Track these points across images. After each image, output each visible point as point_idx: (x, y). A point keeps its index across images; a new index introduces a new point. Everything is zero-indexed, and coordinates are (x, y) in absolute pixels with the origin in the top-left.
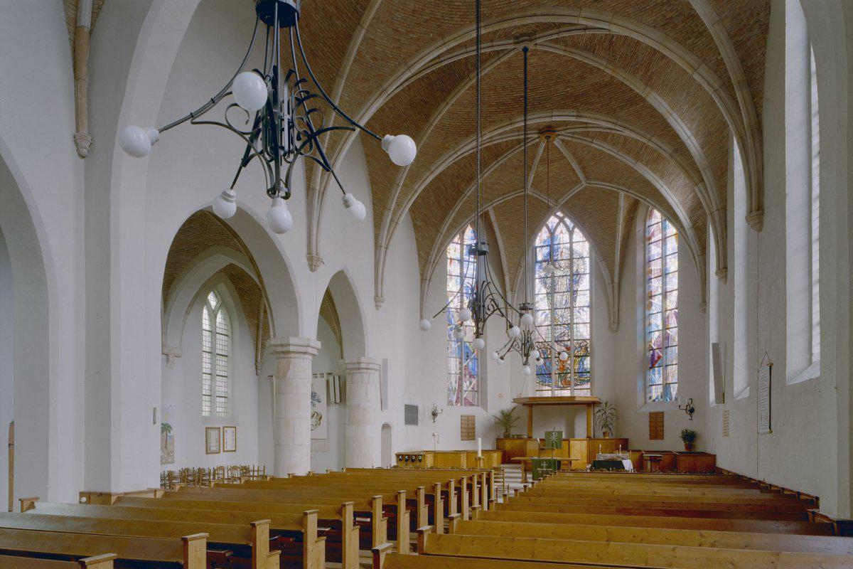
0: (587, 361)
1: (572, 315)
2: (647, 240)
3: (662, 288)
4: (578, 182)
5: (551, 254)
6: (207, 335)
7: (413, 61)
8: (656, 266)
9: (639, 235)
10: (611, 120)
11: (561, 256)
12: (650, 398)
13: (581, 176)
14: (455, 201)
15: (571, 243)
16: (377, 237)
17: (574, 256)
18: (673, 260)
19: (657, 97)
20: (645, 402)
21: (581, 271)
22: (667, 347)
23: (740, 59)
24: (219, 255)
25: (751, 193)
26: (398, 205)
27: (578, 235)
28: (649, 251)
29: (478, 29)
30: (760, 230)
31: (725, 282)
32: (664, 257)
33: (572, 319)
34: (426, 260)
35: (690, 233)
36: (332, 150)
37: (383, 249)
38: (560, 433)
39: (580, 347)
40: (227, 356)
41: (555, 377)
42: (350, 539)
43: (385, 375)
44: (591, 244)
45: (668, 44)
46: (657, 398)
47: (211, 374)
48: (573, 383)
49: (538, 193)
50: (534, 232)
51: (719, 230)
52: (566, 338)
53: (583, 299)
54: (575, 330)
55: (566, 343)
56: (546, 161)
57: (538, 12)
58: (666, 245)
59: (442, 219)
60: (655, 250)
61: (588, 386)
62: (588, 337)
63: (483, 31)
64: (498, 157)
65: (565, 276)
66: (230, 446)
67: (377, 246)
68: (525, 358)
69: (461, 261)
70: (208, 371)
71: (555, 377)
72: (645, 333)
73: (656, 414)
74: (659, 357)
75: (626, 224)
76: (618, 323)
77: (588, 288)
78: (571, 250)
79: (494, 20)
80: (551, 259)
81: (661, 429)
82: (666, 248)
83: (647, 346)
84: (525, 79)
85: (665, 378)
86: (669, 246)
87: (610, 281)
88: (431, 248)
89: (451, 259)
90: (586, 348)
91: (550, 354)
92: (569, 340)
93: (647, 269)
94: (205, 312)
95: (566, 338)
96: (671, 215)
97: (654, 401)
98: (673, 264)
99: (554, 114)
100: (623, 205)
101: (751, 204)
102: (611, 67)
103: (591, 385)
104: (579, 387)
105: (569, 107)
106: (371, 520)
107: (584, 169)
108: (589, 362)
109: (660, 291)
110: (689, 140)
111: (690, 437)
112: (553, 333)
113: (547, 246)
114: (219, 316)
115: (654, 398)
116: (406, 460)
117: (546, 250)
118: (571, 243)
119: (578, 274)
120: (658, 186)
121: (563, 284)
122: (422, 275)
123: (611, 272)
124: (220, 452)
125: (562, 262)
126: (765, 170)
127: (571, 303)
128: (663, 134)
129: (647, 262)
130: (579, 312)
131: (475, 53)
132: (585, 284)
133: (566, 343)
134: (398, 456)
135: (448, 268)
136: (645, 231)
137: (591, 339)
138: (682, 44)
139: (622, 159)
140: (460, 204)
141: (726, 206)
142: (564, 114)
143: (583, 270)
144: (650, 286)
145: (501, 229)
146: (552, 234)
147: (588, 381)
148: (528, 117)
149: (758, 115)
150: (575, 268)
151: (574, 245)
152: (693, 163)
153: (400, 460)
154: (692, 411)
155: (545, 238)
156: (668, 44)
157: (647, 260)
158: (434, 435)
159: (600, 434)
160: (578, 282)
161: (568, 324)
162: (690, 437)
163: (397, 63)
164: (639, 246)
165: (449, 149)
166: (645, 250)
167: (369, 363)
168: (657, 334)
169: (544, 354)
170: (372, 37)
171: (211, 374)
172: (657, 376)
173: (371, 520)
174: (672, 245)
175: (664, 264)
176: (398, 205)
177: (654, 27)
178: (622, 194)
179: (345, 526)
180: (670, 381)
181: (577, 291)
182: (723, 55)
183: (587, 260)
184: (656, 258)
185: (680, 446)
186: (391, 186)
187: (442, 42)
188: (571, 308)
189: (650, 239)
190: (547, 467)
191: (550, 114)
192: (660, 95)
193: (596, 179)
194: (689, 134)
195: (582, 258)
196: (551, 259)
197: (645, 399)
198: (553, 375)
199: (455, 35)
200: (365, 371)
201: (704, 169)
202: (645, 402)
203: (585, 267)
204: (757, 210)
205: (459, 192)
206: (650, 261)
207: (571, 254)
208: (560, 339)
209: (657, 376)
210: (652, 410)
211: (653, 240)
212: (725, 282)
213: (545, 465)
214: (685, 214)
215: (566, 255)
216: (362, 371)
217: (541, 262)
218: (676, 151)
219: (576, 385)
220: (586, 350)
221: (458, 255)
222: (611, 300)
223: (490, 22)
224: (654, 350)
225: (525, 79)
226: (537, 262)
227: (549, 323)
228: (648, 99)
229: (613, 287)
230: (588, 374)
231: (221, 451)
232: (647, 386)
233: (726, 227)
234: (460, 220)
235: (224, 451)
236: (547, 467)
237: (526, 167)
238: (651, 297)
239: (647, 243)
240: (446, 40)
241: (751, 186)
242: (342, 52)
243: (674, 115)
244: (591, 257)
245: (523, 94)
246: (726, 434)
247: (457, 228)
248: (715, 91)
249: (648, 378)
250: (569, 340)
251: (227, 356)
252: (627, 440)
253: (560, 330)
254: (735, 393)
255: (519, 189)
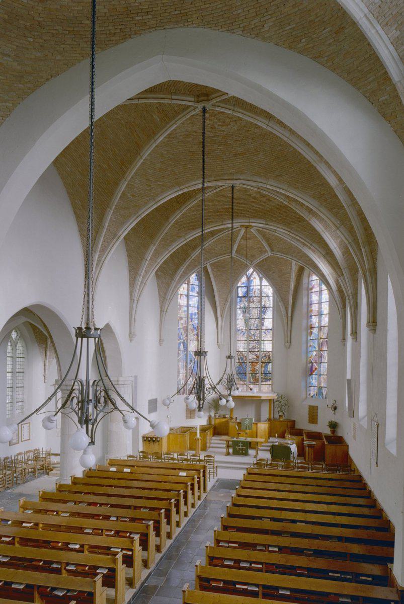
0: (270, 366)
1: (260, 335)
2: (310, 289)
3: (319, 323)
4: (266, 252)
5: (247, 292)
6: (10, 364)
7: (160, 198)
8: (315, 308)
9: (305, 285)
10: (286, 229)
11: (254, 294)
12: (310, 394)
13: (267, 248)
14: (184, 260)
15: (261, 286)
16: (131, 293)
17: (263, 295)
18: (326, 306)
19: (316, 221)
20: (307, 397)
21: (267, 305)
22: (320, 363)
23: (364, 228)
24: (22, 317)
25: (369, 307)
26: (146, 272)
27: (265, 282)
28: (311, 298)
29: (203, 183)
30: (375, 333)
31: (356, 341)
32: (320, 303)
33: (261, 337)
34: (164, 298)
35: (336, 294)
36: (103, 251)
37: (135, 302)
38: (251, 420)
39: (266, 356)
40: (24, 358)
41: (249, 376)
42: (120, 577)
43: (136, 387)
44: (273, 290)
45: (321, 209)
46: (314, 395)
47: (12, 387)
48: (260, 380)
49: (240, 257)
50: (237, 278)
51: (352, 308)
52: (256, 350)
53: (268, 323)
54: (262, 345)
55: (256, 353)
56: (245, 238)
57: (241, 178)
58: (321, 295)
59: (175, 272)
60: (315, 298)
61: (270, 382)
62: (271, 350)
63: (206, 185)
64: (214, 235)
65: (257, 308)
66: (26, 437)
67: (131, 299)
68: (229, 391)
69: (187, 296)
70: (10, 370)
71: (249, 376)
72: (307, 352)
73: (313, 407)
74: (316, 369)
75: (297, 278)
76: (291, 343)
77: (271, 317)
78: (261, 290)
79: (213, 179)
80: (247, 295)
81: (316, 411)
82: (321, 297)
83: (309, 360)
84: (233, 198)
85: (319, 383)
86: (323, 296)
87: (286, 315)
88: (167, 290)
89: (181, 295)
90: (269, 357)
91: (246, 360)
92: (258, 351)
93: (310, 309)
94: (9, 344)
95: (256, 350)
96: (324, 280)
97: (312, 397)
98: (326, 308)
99: (251, 221)
100: (294, 267)
101: (369, 317)
102: (287, 200)
103: (272, 383)
104: (264, 383)
105: (260, 218)
106: (133, 553)
107: (270, 245)
108: (271, 367)
109: (317, 325)
110: (335, 250)
111: (334, 426)
112: (248, 346)
113: (245, 287)
114: (19, 344)
115: (312, 395)
116: (149, 441)
117: (245, 290)
118: (261, 286)
119: (265, 307)
120: (317, 262)
121: (255, 313)
122: (161, 308)
123: (287, 308)
124: (19, 443)
125: (255, 298)
126: (378, 298)
127: (260, 326)
128: (320, 242)
129: (310, 304)
130: (265, 333)
131: (201, 233)
132: (269, 314)
133: (256, 353)
134: (143, 437)
135: (179, 300)
136: (308, 284)
137: (272, 352)
138: (330, 211)
139: (294, 243)
140: (188, 263)
141: (357, 293)
142: (257, 222)
143: (268, 305)
144: (311, 321)
145: (215, 277)
146: (248, 278)
147: (270, 379)
148: (234, 222)
149: (374, 263)
150: (263, 303)
151: (263, 287)
152: (337, 263)
153: (145, 440)
154: (335, 408)
155: (244, 281)
156: (321, 209)
157: (309, 303)
158: (167, 417)
159: (277, 416)
160: (264, 313)
161: (257, 341)
162: (334, 426)
163: (148, 199)
164: (305, 292)
165: (181, 237)
166: (309, 296)
167: (125, 381)
168: (315, 353)
169: (242, 359)
170: (132, 184)
171: (12, 387)
172: (314, 380)
173: (133, 553)
174: (326, 296)
175: (320, 308)
176: (146, 272)
177: (313, 197)
178: (294, 262)
179: (117, 570)
180: (322, 385)
181: (264, 318)
182: (353, 224)
183: (271, 298)
184: (315, 302)
185: (327, 431)
186: (142, 259)
187: (178, 189)
188: (260, 330)
189: (311, 289)
190: (242, 446)
191: (248, 221)
192: (318, 220)
193: (277, 252)
194: (336, 246)
195: (268, 296)
196: (247, 295)
197: (306, 394)
198: (247, 374)
199: (187, 185)
200: (122, 386)
201: (344, 269)
202: (307, 397)
203: (269, 302)
204: (373, 322)
205: (188, 256)
206: (311, 304)
207: (261, 293)
208: (252, 350)
209: (314, 380)
210: (312, 404)
211: (313, 290)
212: (356, 341)
213: (241, 444)
214: (333, 282)
215: (257, 293)
216: (120, 386)
217: (241, 297)
218: (327, 254)
219: (262, 382)
220: (268, 359)
221: (185, 292)
222: (286, 328)
223: (210, 179)
224: (312, 363)
225: (233, 198)
226: (238, 297)
227: (246, 339)
228: (310, 222)
229: (287, 318)
230: (270, 375)
231: (20, 442)
232: (308, 386)
233: (357, 306)
234: (188, 272)
235: (22, 441)
236: (242, 446)
237: (232, 240)
238: (312, 328)
239: (310, 292)
240: (181, 188)
241: (369, 303)
242: (112, 193)
243: (327, 233)
244: (273, 297)
245: (231, 206)
246: (355, 438)
247: (185, 276)
248: (350, 243)
249: (309, 381)
250: (258, 351)
251: (24, 358)
252: (294, 421)
253: (253, 344)
254: (360, 416)
255: (228, 253)
